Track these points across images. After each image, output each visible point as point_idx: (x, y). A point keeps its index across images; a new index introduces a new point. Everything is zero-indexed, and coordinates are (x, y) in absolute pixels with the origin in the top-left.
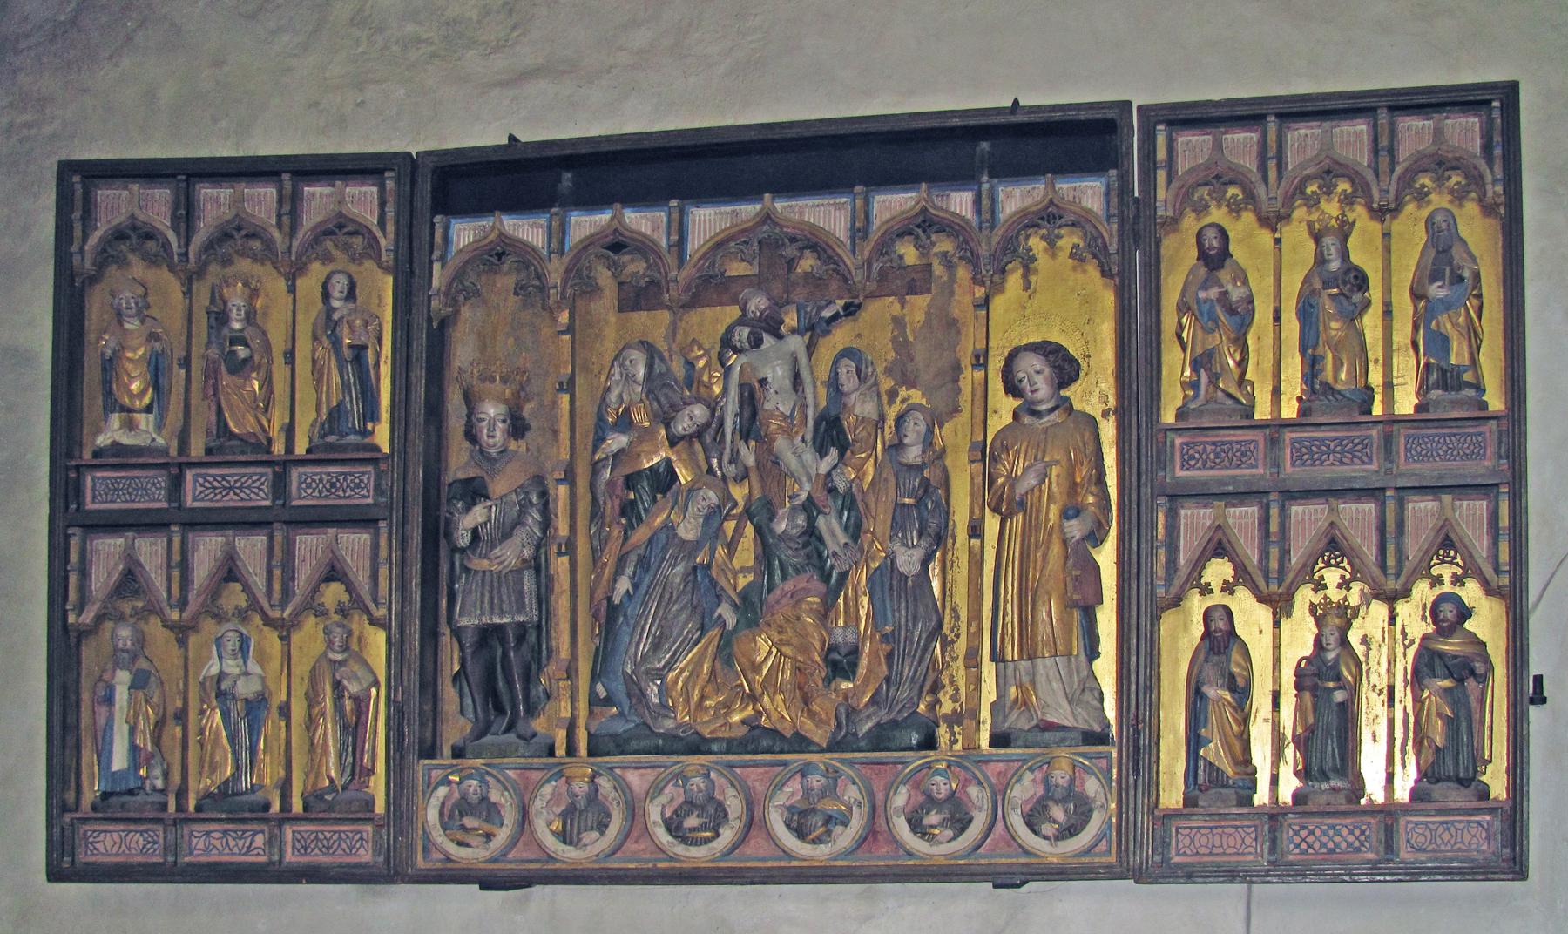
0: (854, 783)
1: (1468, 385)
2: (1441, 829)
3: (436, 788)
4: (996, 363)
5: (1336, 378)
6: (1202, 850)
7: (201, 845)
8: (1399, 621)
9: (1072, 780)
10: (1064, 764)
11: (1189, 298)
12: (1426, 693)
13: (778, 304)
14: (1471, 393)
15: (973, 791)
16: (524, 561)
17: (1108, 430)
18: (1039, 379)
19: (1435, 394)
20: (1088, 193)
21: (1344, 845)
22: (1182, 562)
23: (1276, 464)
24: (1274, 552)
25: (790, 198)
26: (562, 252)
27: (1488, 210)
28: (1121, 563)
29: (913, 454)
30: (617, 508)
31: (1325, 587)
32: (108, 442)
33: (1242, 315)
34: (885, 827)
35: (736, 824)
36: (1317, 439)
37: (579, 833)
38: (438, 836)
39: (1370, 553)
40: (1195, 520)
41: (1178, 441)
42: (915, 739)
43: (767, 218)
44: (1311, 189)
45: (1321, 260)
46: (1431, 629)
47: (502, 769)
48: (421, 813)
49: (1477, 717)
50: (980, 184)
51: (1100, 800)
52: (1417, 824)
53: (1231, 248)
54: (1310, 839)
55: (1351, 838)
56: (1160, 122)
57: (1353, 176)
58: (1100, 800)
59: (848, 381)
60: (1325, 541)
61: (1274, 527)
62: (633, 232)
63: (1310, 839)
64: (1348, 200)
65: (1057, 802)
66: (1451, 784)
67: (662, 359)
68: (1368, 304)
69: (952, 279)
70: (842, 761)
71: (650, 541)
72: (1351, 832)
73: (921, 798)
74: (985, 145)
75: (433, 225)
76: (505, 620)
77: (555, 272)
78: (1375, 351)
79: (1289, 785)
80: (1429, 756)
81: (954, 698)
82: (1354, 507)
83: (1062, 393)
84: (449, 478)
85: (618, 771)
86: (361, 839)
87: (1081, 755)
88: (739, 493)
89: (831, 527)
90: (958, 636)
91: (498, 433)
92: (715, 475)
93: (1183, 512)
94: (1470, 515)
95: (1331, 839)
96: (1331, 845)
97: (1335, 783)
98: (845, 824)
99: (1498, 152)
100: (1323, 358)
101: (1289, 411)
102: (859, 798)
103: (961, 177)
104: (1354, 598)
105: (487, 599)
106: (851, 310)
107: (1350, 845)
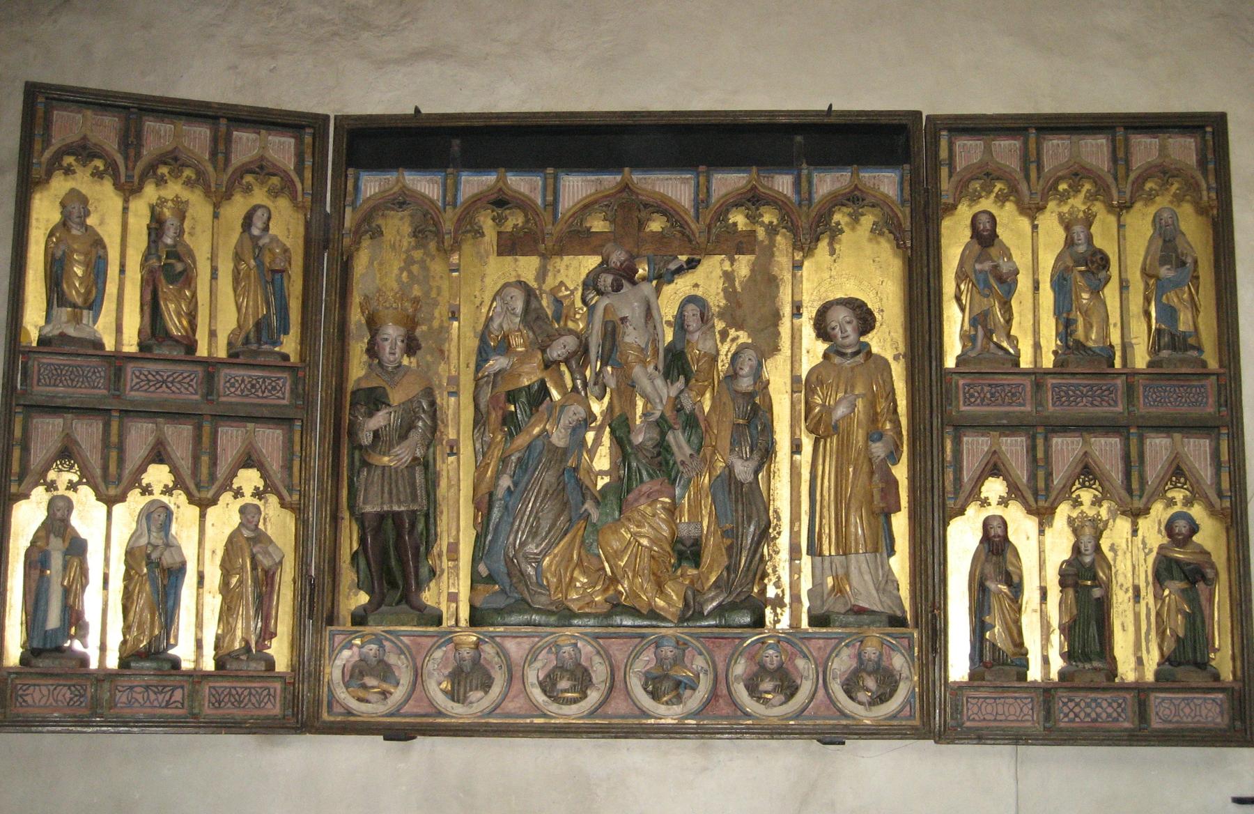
0: (701, 654)
1: (1193, 347)
2: (1183, 705)
3: (341, 651)
4: (809, 313)
5: (1087, 337)
6: (988, 717)
7: (124, 699)
8: (1140, 533)
9: (881, 654)
10: (875, 642)
11: (967, 268)
12: (1167, 592)
13: (633, 258)
14: (1195, 353)
15: (801, 663)
16: (415, 459)
17: (898, 372)
18: (849, 328)
19: (1165, 353)
20: (886, 182)
21: (1104, 715)
22: (966, 479)
23: (1039, 403)
24: (1041, 474)
25: (645, 172)
26: (454, 205)
27: (1201, 211)
28: (912, 479)
29: (745, 384)
30: (500, 418)
31: (1081, 504)
32: (56, 332)
33: (1007, 282)
34: (725, 692)
35: (602, 686)
36: (1072, 385)
37: (465, 692)
38: (342, 694)
39: (1117, 477)
40: (976, 447)
41: (961, 382)
42: (747, 620)
43: (626, 187)
44: (1063, 187)
45: (1070, 243)
46: (1166, 540)
47: (397, 634)
48: (327, 670)
49: (1207, 612)
50: (800, 171)
51: (905, 673)
52: (1163, 699)
53: (999, 231)
54: (1077, 710)
55: (1110, 710)
56: (945, 129)
57: (1097, 180)
58: (905, 673)
59: (693, 322)
60: (1081, 466)
61: (1040, 455)
62: (515, 192)
63: (1077, 710)
64: (1091, 197)
65: (869, 674)
66: (1188, 667)
67: (536, 297)
68: (1108, 279)
69: (772, 244)
70: (691, 635)
71: (529, 446)
72: (1110, 705)
73: (755, 668)
74: (799, 138)
75: (346, 176)
76: (403, 509)
77: (448, 221)
78: (1114, 317)
79: (1057, 664)
80: (1169, 646)
81: (777, 585)
82: (1103, 440)
83: (862, 339)
84: (350, 386)
85: (498, 639)
86: (269, 694)
87: (888, 635)
88: (597, 408)
89: (679, 441)
90: (779, 533)
91: (398, 350)
92: (579, 393)
93: (965, 439)
94: (1197, 451)
95: (1093, 710)
96: (1093, 715)
97: (1096, 664)
98: (694, 689)
99: (1211, 166)
100: (1075, 321)
101: (1048, 362)
102: (705, 666)
103: (783, 162)
104: (1104, 512)
105: (386, 489)
106: (692, 264)
107: (1109, 716)
